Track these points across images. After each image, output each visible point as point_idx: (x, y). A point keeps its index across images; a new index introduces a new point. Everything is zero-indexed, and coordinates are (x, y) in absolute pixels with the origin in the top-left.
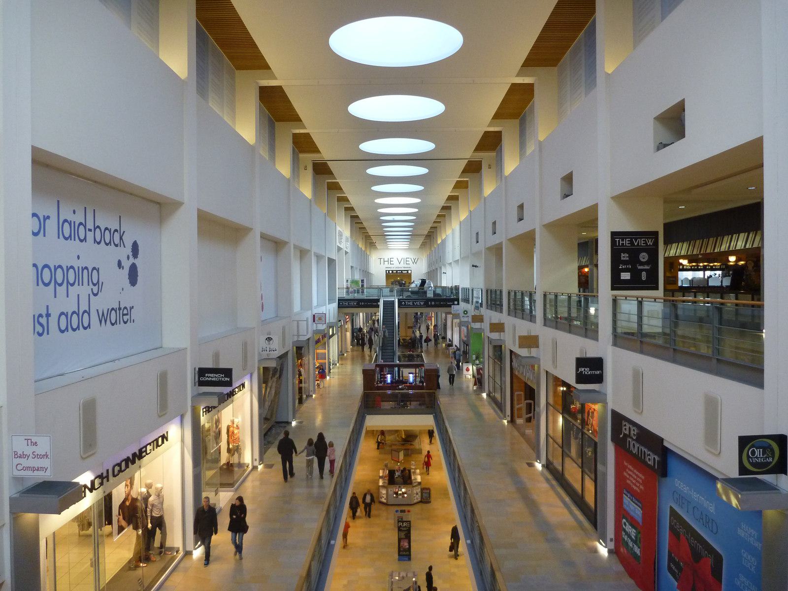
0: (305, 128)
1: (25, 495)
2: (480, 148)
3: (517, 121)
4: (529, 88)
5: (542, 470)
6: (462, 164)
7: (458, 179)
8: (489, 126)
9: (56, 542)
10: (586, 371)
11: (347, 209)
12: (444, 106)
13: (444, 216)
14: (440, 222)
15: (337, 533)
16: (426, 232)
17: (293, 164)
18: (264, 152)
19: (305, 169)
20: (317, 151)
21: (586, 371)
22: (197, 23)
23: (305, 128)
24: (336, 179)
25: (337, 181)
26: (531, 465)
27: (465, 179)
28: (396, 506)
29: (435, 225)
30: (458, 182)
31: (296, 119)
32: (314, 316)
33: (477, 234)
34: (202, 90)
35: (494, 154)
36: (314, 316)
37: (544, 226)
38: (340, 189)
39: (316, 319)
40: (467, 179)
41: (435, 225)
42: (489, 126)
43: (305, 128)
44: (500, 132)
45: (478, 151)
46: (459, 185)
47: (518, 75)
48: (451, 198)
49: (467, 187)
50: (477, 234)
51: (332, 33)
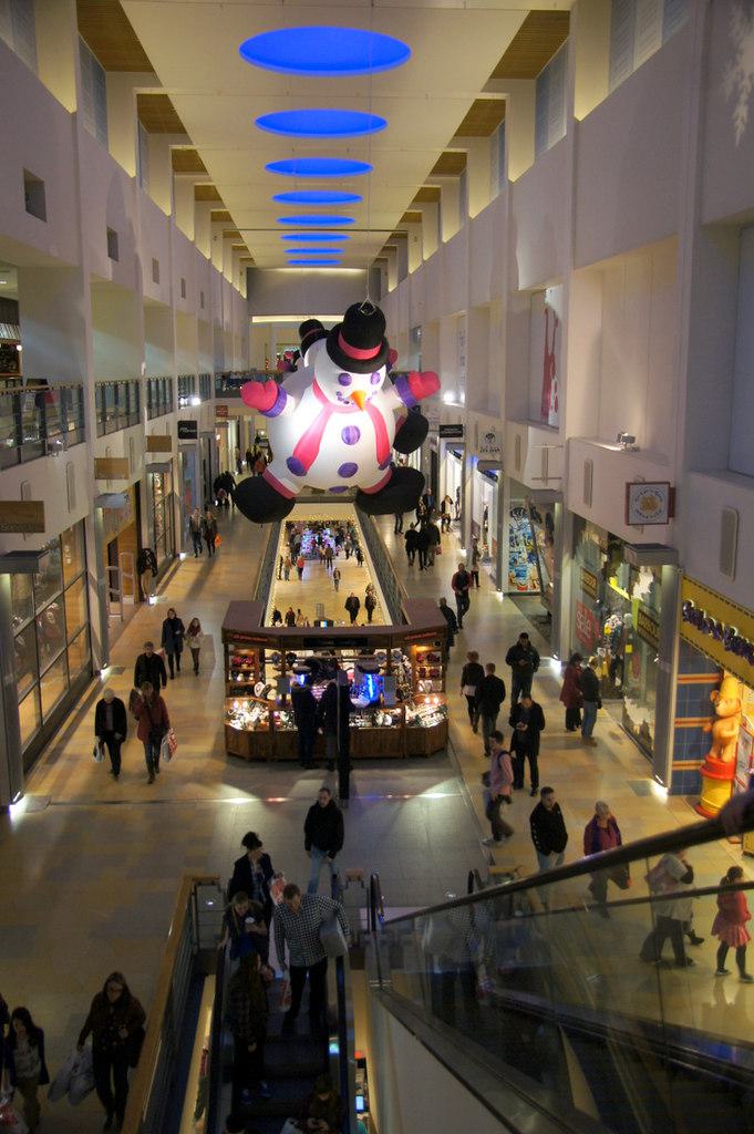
1: (199, 477)
3: (532, 83)
4: (500, 104)
5: (669, 799)
7: (449, 150)
9: (135, 532)
10: (185, 430)
11: (235, 248)
17: (140, 144)
18: (89, 127)
21: (185, 430)
26: (644, 792)
30: (422, 190)
32: (672, 513)
35: (456, 179)
36: (672, 513)
38: (226, 220)
39: (663, 505)
45: (467, 135)
47: (483, 91)
49: (420, 221)
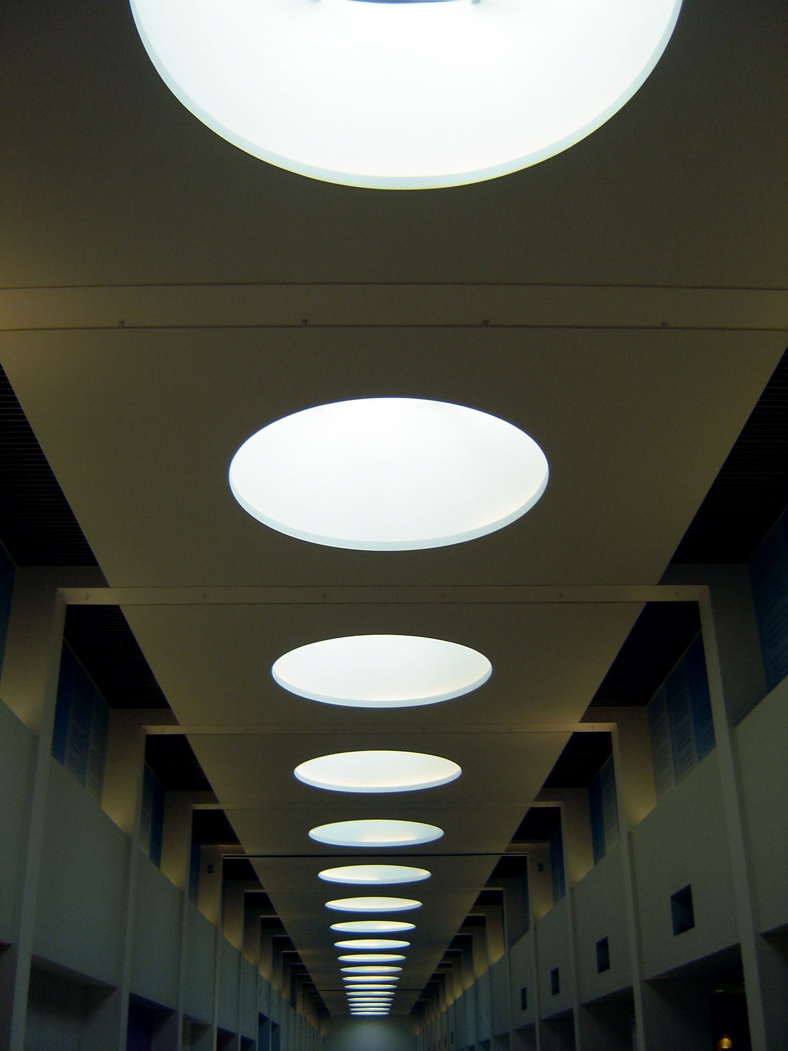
0: (174, 722)
2: (521, 835)
6: (491, 865)
7: (483, 889)
8: (538, 799)
12: (460, 768)
13: (457, 954)
14: (450, 966)
15: (353, 980)
16: (423, 986)
18: (143, 848)
19: (210, 872)
20: (234, 840)
22: (64, 642)
23: (175, 723)
24: (276, 914)
25: (289, 936)
27: (496, 889)
28: (347, 854)
29: (442, 971)
30: (483, 894)
31: (202, 786)
33: (524, 991)
34: (58, 749)
35: (546, 845)
37: (646, 981)
40: (500, 889)
41: (442, 971)
42: (538, 799)
43: (174, 722)
44: (556, 810)
46: (485, 899)
48: (470, 922)
50: (524, 991)
51: (298, 765)
